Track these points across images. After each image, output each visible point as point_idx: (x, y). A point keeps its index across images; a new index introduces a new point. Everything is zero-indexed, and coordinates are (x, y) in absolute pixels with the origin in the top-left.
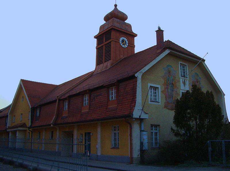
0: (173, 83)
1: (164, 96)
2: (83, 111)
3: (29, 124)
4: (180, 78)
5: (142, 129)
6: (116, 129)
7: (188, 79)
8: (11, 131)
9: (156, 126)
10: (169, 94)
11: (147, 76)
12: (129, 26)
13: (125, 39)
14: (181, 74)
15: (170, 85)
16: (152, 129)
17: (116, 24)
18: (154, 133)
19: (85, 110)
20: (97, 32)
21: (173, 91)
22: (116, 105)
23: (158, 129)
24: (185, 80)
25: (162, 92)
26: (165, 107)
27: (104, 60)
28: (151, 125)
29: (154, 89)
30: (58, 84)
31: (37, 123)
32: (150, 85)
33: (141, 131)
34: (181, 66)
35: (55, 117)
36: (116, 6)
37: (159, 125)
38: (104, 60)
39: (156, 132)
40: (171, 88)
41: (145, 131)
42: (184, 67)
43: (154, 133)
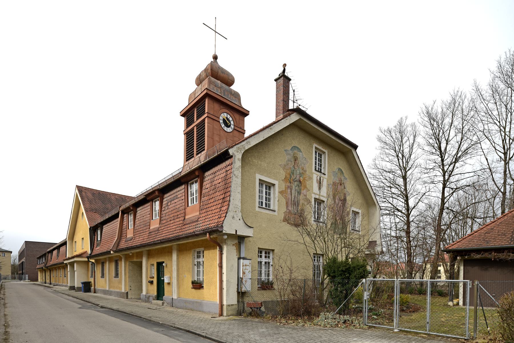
0: (301, 181)
1: (284, 201)
2: (151, 228)
3: (89, 252)
4: (312, 173)
5: (242, 255)
6: (200, 255)
7: (326, 176)
8: (69, 263)
9: (268, 252)
10: (293, 198)
11: (254, 160)
12: (237, 96)
13: (229, 117)
14: (316, 167)
15: (296, 183)
16: (261, 257)
17: (218, 91)
18: (263, 263)
19: (155, 225)
20: (184, 104)
21: (299, 193)
22: (198, 213)
23: (271, 257)
24: (322, 179)
25: (281, 192)
26: (285, 220)
27: (195, 153)
28: (259, 248)
29: (266, 186)
30: (133, 196)
31: (98, 250)
32: (258, 177)
33: (239, 258)
34: (316, 152)
35: (116, 239)
36: (215, 58)
37: (273, 250)
38: (195, 153)
39: (267, 261)
40: (297, 188)
41: (248, 258)
42: (321, 155)
43: (263, 263)
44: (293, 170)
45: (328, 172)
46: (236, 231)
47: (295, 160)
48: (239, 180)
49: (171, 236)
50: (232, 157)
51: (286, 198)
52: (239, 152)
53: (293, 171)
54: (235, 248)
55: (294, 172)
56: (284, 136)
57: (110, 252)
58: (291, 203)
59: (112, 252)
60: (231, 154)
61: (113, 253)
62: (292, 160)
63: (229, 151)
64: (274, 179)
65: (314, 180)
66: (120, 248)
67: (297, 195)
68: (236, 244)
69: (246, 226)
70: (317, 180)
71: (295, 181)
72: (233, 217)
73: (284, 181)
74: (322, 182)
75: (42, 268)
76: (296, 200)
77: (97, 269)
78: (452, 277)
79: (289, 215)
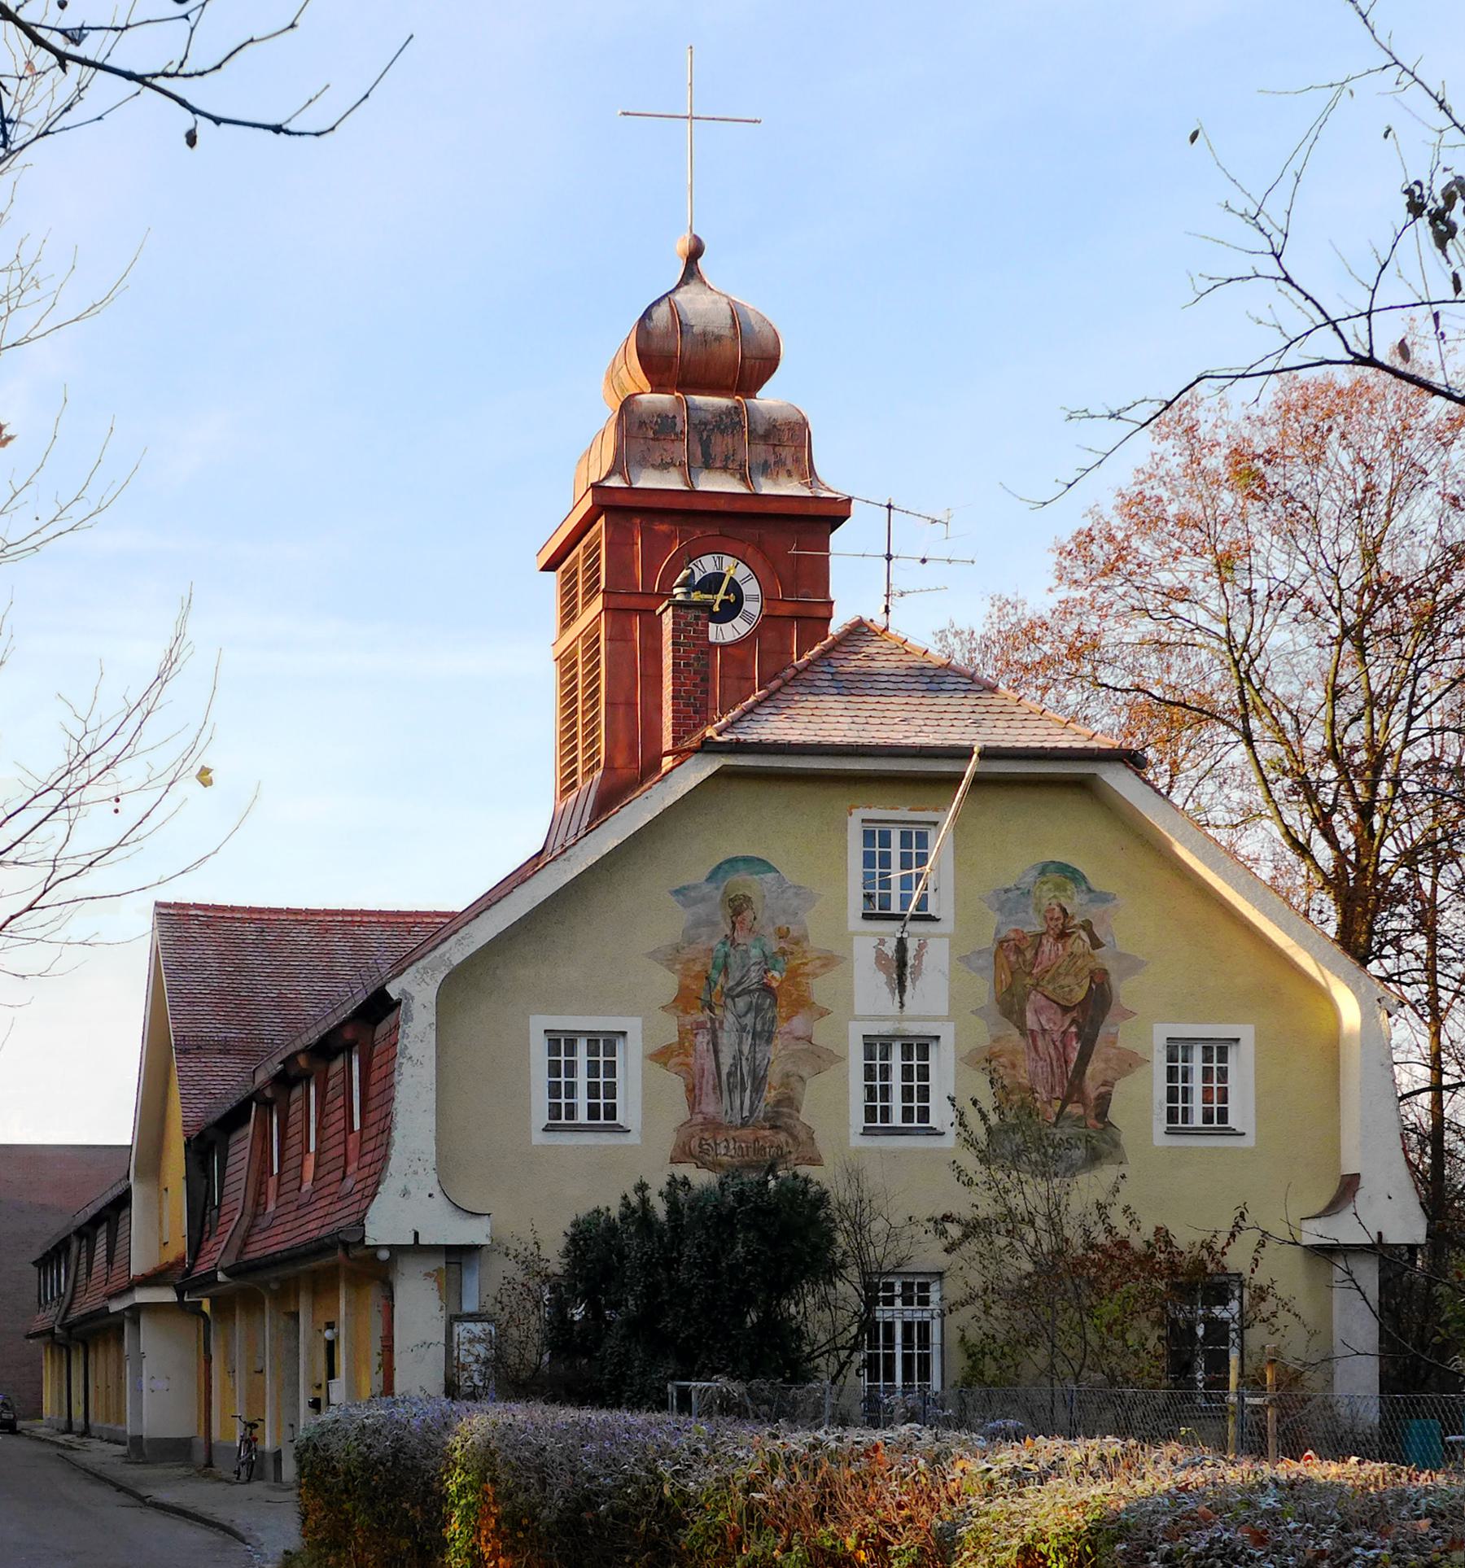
40: (749, 1020)
44: (721, 954)
46: (416, 1234)
47: (737, 912)
48: (428, 1072)
49: (298, 1240)
50: (399, 1003)
51: (685, 1070)
52: (427, 980)
53: (727, 955)
55: (731, 960)
57: (215, 1273)
58: (718, 1087)
59: (221, 1277)
60: (395, 998)
63: (388, 988)
64: (620, 1014)
66: (202, 1267)
67: (753, 1045)
68: (438, 1270)
70: (880, 956)
71: (738, 996)
72: (405, 1193)
73: (676, 1007)
75: (51, 1331)
77: (228, 1359)
79: (706, 1135)
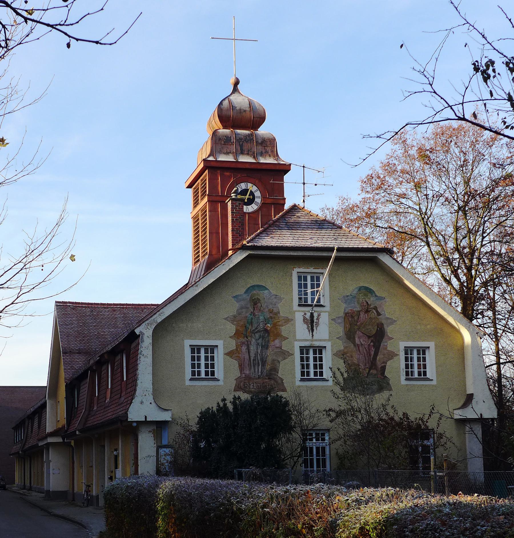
24: (316, 315)
40: (260, 341)
45: (332, 300)
46: (146, 417)
48: (149, 360)
51: (238, 359)
53: (252, 319)
54: (153, 435)
55: (253, 320)
56: (232, 280)
59: (77, 433)
61: (80, 434)
62: (249, 306)
64: (215, 339)
65: (296, 322)
69: (163, 410)
70: (305, 319)
71: (256, 333)
74: (317, 319)
76: (259, 358)
78: (318, 471)
